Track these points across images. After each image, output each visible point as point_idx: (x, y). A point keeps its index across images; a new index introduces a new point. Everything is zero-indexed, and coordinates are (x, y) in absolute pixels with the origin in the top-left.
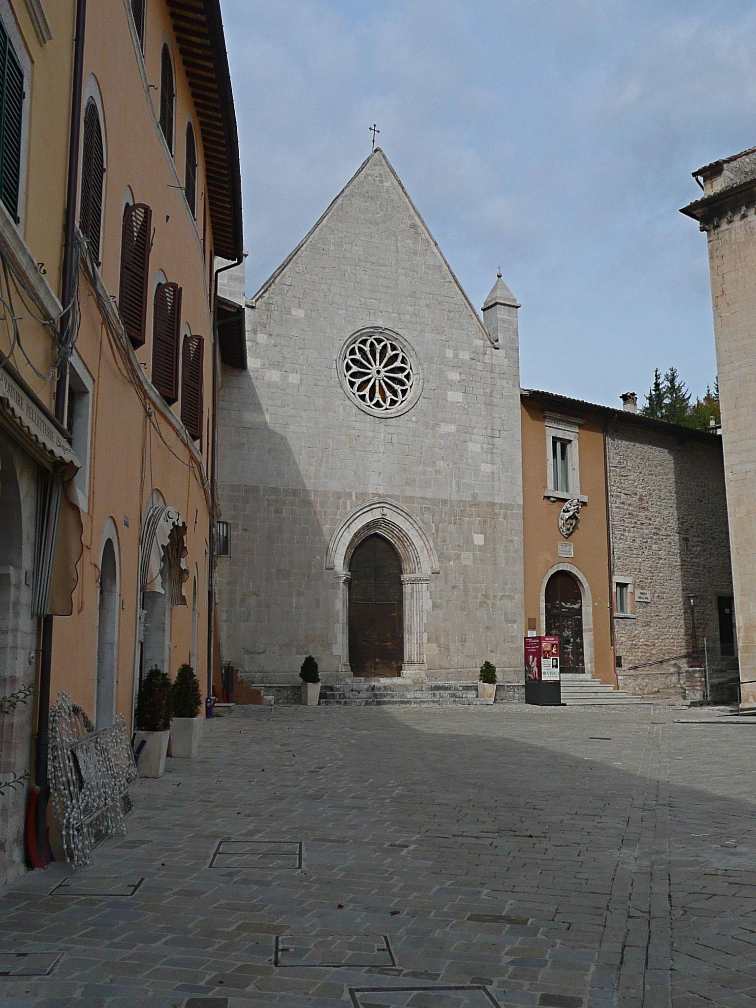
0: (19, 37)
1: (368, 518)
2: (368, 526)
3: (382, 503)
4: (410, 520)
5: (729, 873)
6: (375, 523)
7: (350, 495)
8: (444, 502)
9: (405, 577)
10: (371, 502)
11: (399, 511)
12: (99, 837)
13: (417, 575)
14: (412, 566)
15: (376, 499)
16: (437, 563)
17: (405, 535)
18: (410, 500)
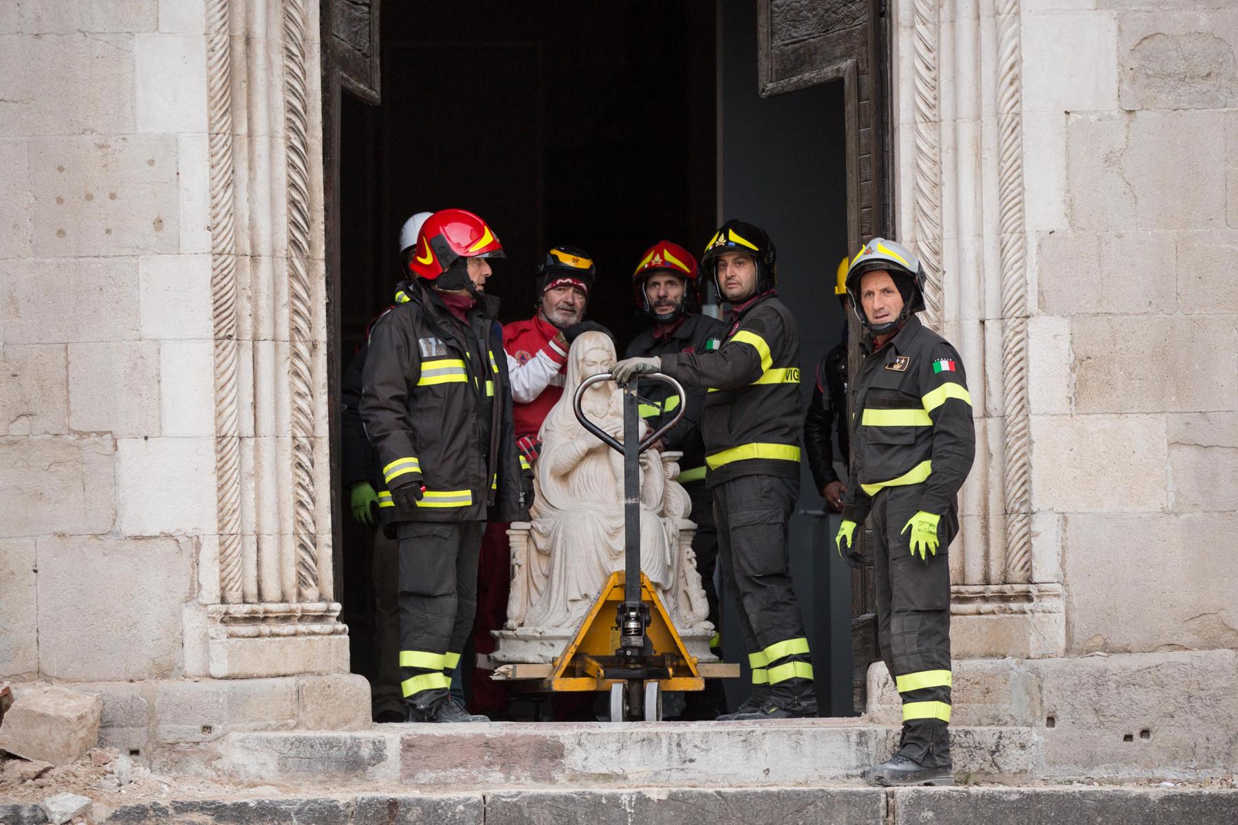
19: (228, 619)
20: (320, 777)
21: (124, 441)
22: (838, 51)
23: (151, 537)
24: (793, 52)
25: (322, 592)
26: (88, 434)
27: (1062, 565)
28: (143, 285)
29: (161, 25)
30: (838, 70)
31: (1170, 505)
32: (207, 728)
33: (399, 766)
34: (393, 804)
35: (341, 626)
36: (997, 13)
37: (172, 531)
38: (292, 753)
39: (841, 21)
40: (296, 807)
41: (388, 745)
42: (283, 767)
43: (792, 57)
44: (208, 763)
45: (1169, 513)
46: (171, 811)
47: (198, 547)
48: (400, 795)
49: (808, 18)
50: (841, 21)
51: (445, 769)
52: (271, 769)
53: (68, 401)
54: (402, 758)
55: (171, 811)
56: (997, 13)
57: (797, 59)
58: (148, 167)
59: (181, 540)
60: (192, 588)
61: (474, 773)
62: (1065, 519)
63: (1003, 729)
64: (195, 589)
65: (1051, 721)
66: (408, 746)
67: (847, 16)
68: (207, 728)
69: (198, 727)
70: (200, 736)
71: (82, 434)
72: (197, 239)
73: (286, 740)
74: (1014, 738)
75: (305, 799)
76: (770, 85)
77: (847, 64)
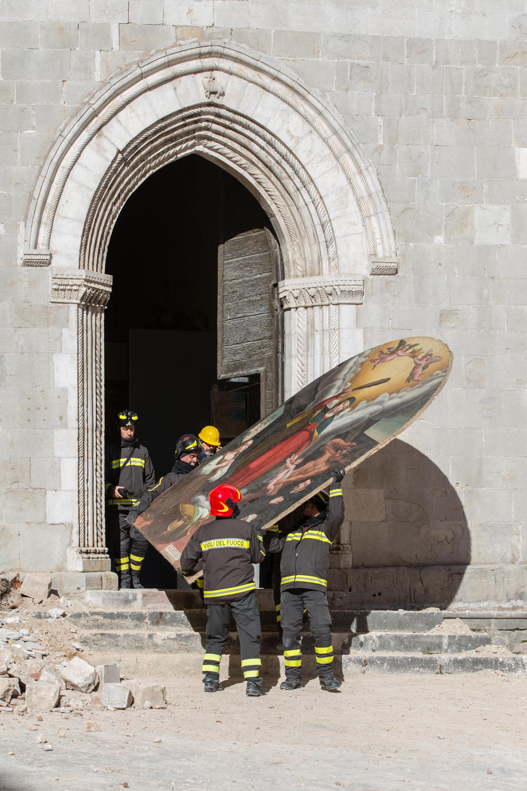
0: (251, 77)
1: (162, 103)
2: (162, 131)
3: (208, 54)
4: (303, 107)
5: (328, 228)
6: (188, 121)
7: (101, 34)
8: (419, 47)
9: (288, 286)
10: (174, 53)
11: (266, 81)
12: (120, 661)
13: (328, 278)
14: (311, 251)
15: (190, 46)
16: (391, 242)
17: (288, 156)
18: (306, 42)
19: (81, 552)
20: (116, 606)
21: (49, 491)
22: (256, 365)
23: (57, 524)
24: (233, 364)
25: (102, 546)
26: (37, 489)
27: (350, 538)
28: (55, 439)
29: (63, 350)
30: (257, 371)
31: (384, 518)
32: (79, 588)
33: (141, 602)
34: (161, 614)
35: (108, 556)
36: (331, 353)
37: (64, 522)
38: (107, 597)
39: (256, 354)
40: (129, 614)
41: (138, 595)
42: (104, 602)
43: (233, 366)
44: (79, 600)
45: (384, 521)
46: (89, 615)
47: (72, 528)
48: (163, 611)
49: (241, 353)
50: (256, 354)
51: (156, 603)
52: (100, 603)
53: (30, 478)
54: (143, 599)
55: (89, 615)
56: (331, 353)
57: (235, 367)
58: (58, 399)
59: (67, 525)
60: (70, 541)
61: (166, 605)
62: (351, 523)
63: (335, 592)
64: (71, 541)
65: (350, 590)
66: (144, 595)
67: (260, 353)
68: (79, 588)
69: (76, 588)
70: (76, 591)
71: (35, 489)
72: (73, 423)
73: (105, 593)
74: (339, 595)
75: (131, 612)
76: (223, 375)
77: (262, 369)
